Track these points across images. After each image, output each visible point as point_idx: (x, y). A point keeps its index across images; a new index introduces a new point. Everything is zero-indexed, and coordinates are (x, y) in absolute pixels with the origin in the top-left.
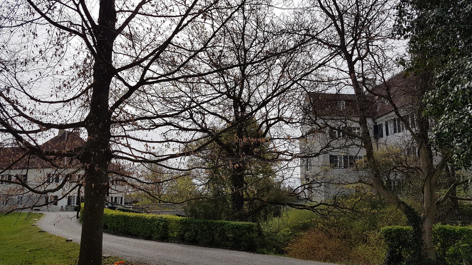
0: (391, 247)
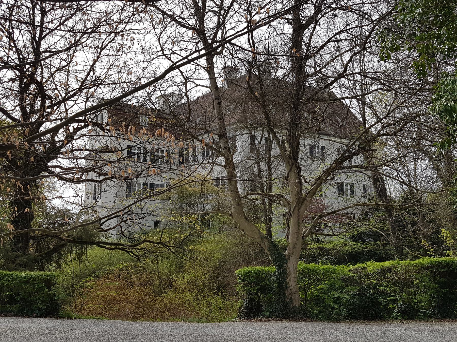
0: (250, 294)
